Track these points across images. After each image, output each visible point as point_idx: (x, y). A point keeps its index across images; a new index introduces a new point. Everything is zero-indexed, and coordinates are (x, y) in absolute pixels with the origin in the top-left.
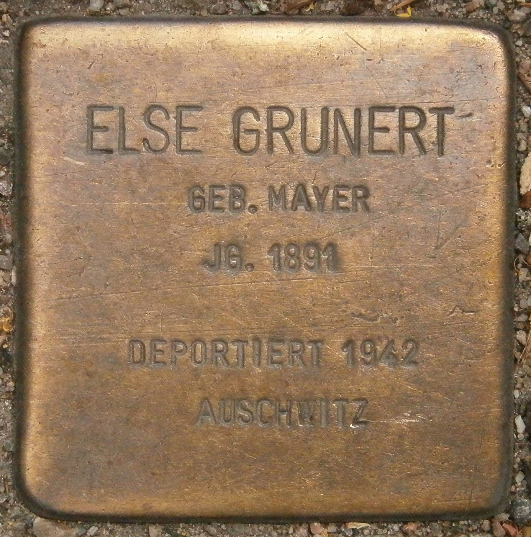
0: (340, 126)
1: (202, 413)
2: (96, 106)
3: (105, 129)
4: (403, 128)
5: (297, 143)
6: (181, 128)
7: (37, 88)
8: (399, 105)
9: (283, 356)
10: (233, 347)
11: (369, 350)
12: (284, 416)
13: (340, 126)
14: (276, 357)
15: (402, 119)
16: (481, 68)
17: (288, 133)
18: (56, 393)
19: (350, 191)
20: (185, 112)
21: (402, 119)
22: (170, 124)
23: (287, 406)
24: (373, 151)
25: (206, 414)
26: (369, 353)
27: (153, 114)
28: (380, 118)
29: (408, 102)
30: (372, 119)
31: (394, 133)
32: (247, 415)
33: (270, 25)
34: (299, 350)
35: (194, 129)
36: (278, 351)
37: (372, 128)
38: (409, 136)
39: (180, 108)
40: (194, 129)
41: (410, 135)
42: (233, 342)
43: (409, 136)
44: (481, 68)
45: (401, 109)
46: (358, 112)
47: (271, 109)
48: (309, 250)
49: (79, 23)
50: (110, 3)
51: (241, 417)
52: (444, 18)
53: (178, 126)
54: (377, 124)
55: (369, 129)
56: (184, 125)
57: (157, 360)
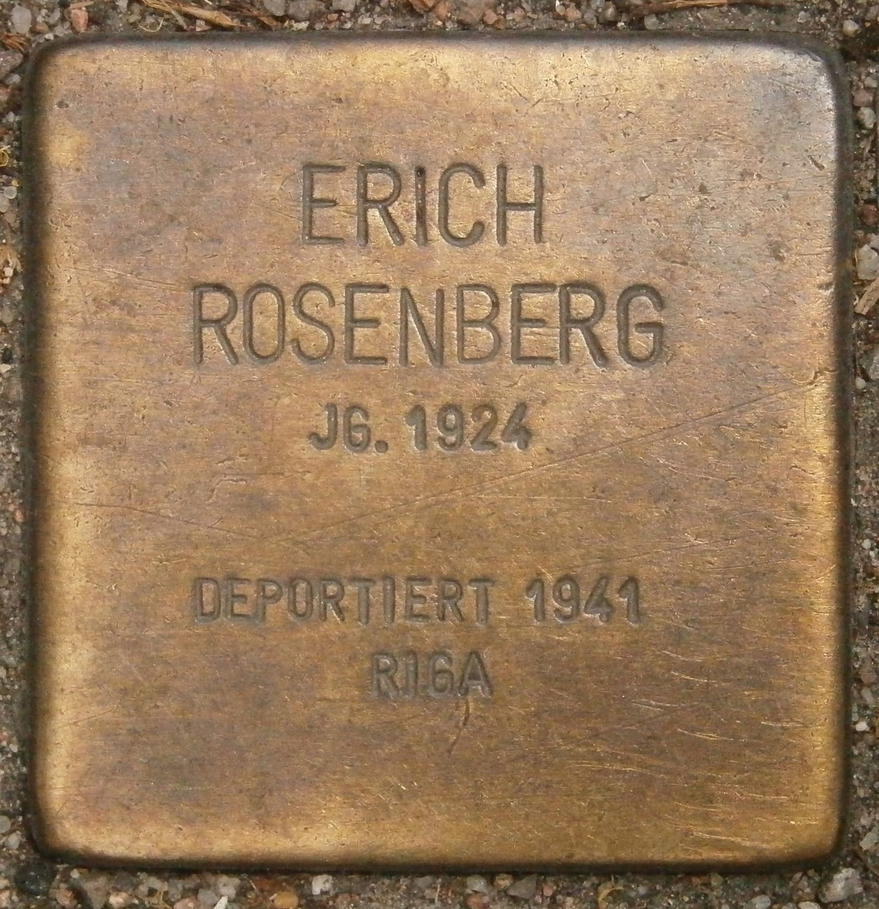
0: (411, 319)
1: (467, 676)
3: (539, 322)
4: (569, 321)
5: (611, 344)
6: (353, 321)
8: (560, 281)
11: (566, 595)
13: (411, 319)
14: (418, 606)
15: (566, 304)
20: (358, 296)
21: (566, 304)
22: (338, 317)
25: (474, 677)
26: (568, 600)
28: (534, 302)
29: (573, 273)
31: (391, 329)
38: (209, 333)
43: (209, 333)
45: (565, 286)
50: (624, 14)
53: (515, 319)
57: (236, 611)
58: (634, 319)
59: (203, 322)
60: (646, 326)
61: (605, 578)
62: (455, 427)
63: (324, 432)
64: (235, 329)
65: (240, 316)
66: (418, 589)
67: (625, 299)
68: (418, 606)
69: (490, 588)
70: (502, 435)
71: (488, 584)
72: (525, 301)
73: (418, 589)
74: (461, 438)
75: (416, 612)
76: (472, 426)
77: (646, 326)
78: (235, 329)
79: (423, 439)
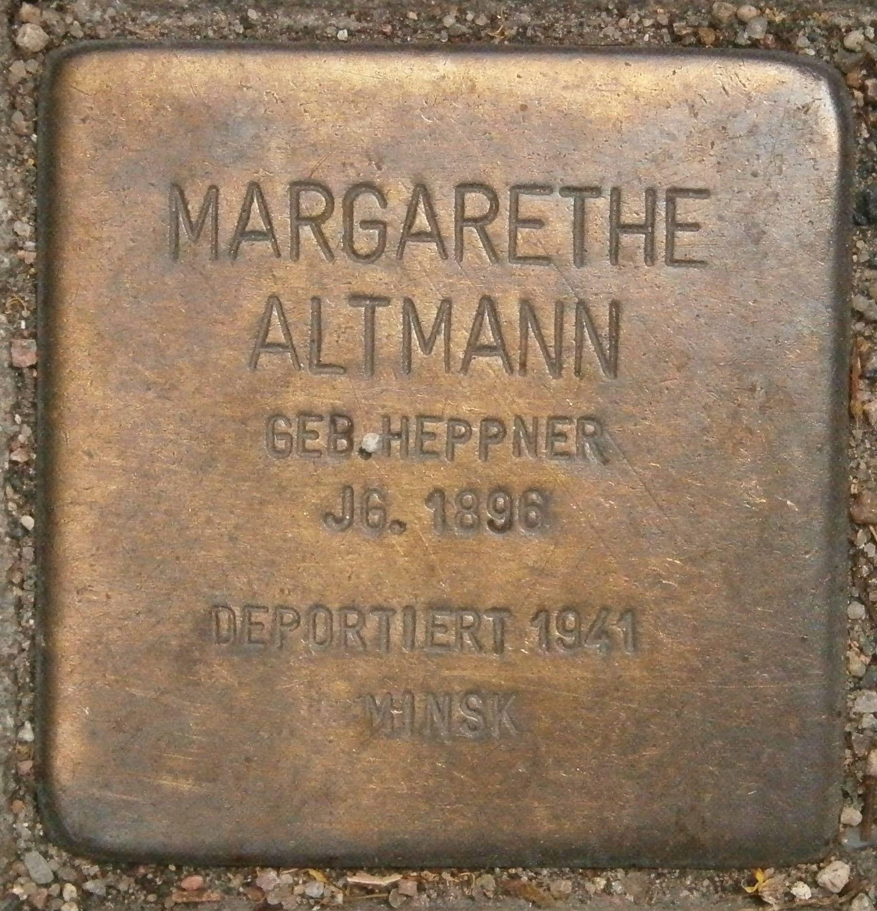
10: (489, 619)
17: (490, 229)
18: (118, 727)
24: (672, 261)
27: (360, 198)
33: (641, 64)
34: (473, 625)
35: (695, 226)
37: (674, 225)
38: (306, 231)
39: (518, 189)
40: (695, 226)
41: (307, 229)
42: (488, 611)
43: (306, 231)
47: (463, 187)
49: (479, 55)
52: (227, 41)
55: (456, 221)
56: (679, 218)
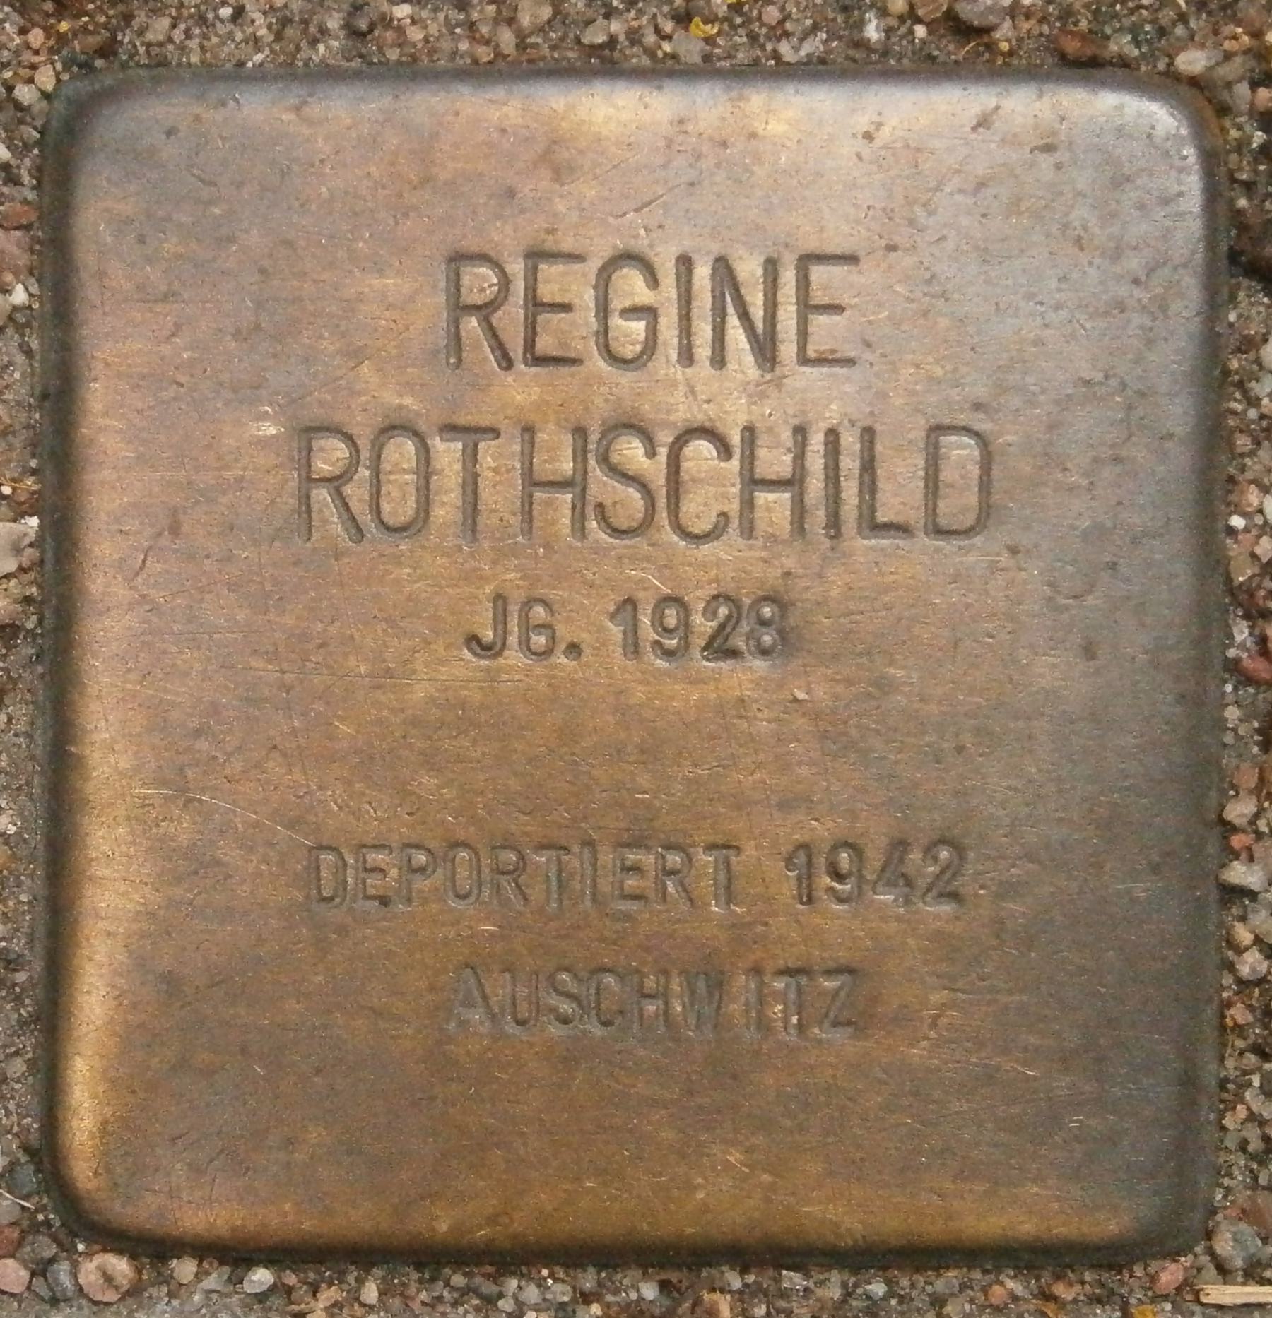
0: (730, 310)
2: (656, 317)
7: (1042, 670)
9: (931, 221)
12: (651, 1008)
13: (730, 310)
14: (631, 883)
16: (473, 640)
19: (497, 908)
23: (658, 984)
30: (803, 283)
32: (566, 1007)
36: (636, 869)
37: (807, 307)
38: (322, 495)
43: (322, 495)
44: (473, 640)
46: (772, 267)
48: (718, 607)
51: (554, 1010)
54: (818, 297)
58: (617, 304)
59: (309, 479)
60: (634, 311)
61: (900, 845)
62: (676, 628)
63: (488, 635)
64: (357, 492)
65: (364, 473)
66: (632, 857)
67: (605, 275)
68: (631, 883)
69: (733, 859)
70: (704, 614)
71: (731, 852)
72: (466, 281)
73: (632, 857)
74: (686, 644)
75: (627, 891)
76: (703, 626)
77: (634, 311)
78: (357, 492)
79: (633, 647)
